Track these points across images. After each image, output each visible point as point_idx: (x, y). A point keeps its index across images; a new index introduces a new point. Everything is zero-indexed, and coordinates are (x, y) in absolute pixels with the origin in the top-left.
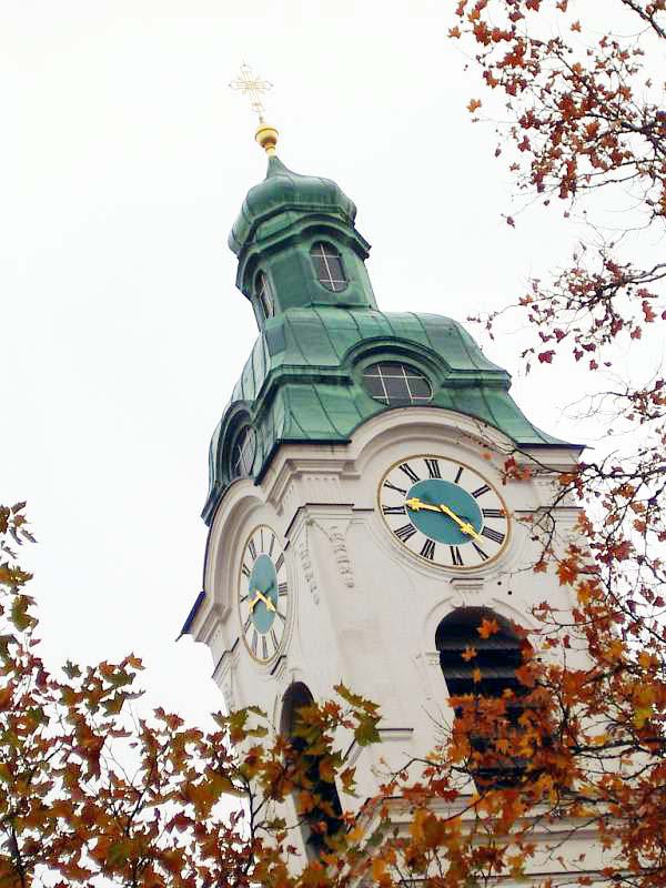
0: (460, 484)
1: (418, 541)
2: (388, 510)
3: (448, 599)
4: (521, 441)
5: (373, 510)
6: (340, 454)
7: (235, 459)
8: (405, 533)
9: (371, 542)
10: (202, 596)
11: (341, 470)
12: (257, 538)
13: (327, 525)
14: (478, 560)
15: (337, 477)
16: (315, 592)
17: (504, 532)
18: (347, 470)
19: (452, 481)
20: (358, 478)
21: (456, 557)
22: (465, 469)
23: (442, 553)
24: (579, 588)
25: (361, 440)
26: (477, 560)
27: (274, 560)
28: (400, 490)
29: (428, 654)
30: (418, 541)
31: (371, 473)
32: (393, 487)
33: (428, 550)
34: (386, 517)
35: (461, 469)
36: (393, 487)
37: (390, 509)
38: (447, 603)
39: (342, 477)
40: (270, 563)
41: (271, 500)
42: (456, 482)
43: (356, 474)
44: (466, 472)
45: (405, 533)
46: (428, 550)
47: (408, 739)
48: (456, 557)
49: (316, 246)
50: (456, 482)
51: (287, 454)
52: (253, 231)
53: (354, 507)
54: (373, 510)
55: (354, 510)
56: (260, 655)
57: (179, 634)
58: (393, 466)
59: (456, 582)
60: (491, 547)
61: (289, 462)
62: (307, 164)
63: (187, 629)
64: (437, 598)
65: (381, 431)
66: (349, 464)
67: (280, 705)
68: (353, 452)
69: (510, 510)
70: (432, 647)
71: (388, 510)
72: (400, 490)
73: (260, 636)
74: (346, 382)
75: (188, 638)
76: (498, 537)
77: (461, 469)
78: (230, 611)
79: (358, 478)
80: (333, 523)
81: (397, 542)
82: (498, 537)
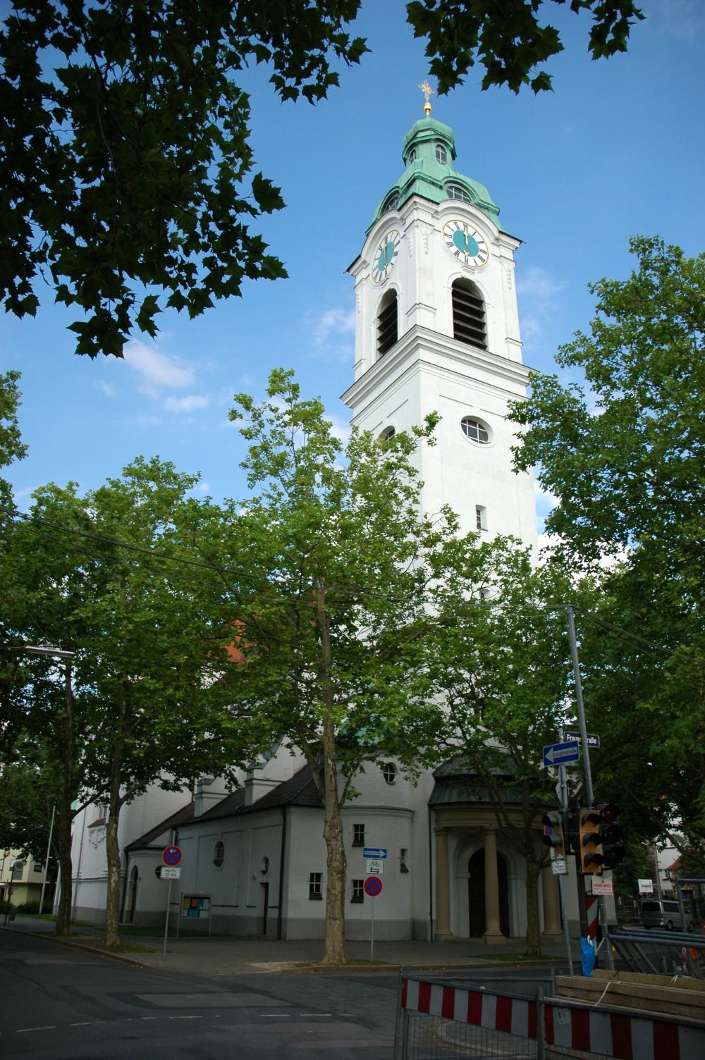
1: (454, 249)
6: (434, 206)
8: (450, 245)
9: (439, 243)
12: (389, 236)
13: (423, 229)
14: (474, 264)
21: (467, 261)
23: (462, 256)
24: (341, 446)
25: (443, 206)
27: (395, 243)
33: (457, 254)
40: (393, 250)
45: (450, 245)
49: (439, 146)
51: (416, 199)
52: (415, 135)
56: (377, 280)
60: (480, 263)
61: (415, 202)
62: (322, 401)
64: (457, 271)
67: (381, 298)
68: (440, 208)
69: (490, 252)
70: (450, 286)
74: (441, 187)
76: (483, 260)
81: (446, 245)
82: (483, 260)
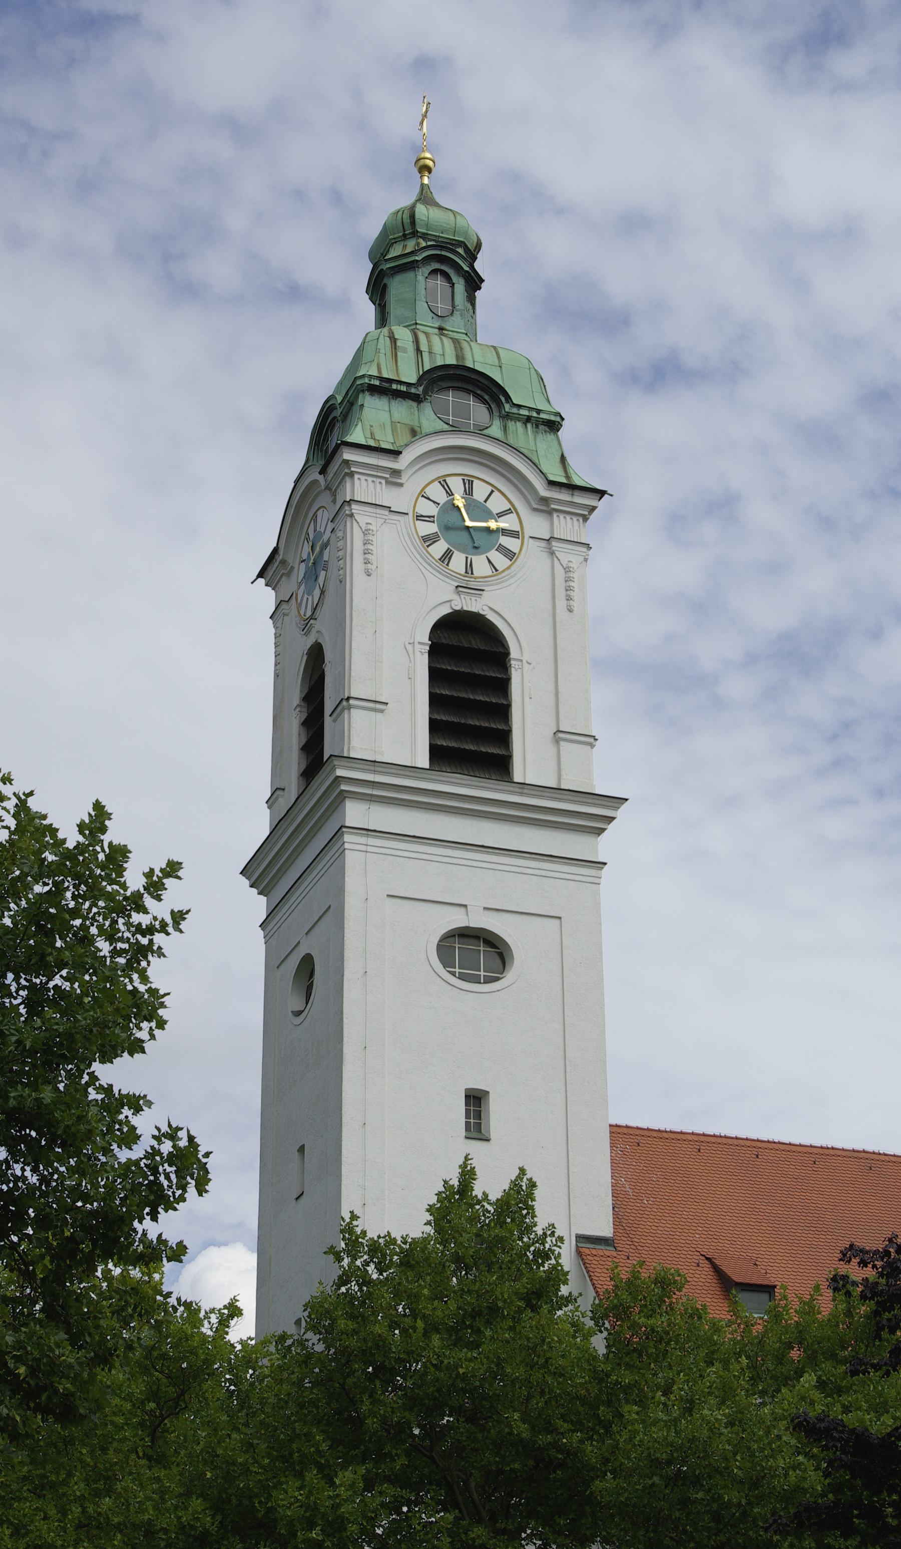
0: (488, 504)
1: (440, 548)
2: (419, 517)
3: (450, 601)
4: (552, 478)
5: (407, 514)
7: (326, 439)
10: (275, 551)
11: (388, 476)
14: (488, 571)
15: (383, 482)
16: (278, 657)
17: (516, 550)
18: (394, 478)
19: (482, 500)
20: (401, 485)
21: (469, 567)
22: (496, 493)
23: (458, 561)
26: (487, 571)
28: (434, 502)
29: (420, 643)
30: (440, 548)
31: (413, 482)
32: (428, 499)
33: (447, 557)
34: (418, 523)
35: (492, 491)
36: (428, 499)
37: (447, 492)
38: (448, 604)
39: (388, 483)
41: (328, 488)
42: (485, 501)
43: (399, 481)
44: (496, 493)
45: (429, 540)
46: (447, 557)
47: (382, 711)
48: (469, 567)
50: (485, 501)
53: (392, 509)
54: (407, 514)
55: (390, 511)
56: (302, 612)
57: (255, 577)
58: (417, 499)
59: (460, 589)
60: (500, 561)
63: (261, 575)
65: (426, 450)
66: (396, 473)
68: (402, 463)
71: (419, 517)
72: (434, 502)
73: (306, 596)
75: (261, 581)
76: (510, 555)
77: (492, 491)
78: (292, 568)
79: (401, 485)
80: (369, 520)
82: (510, 555)
